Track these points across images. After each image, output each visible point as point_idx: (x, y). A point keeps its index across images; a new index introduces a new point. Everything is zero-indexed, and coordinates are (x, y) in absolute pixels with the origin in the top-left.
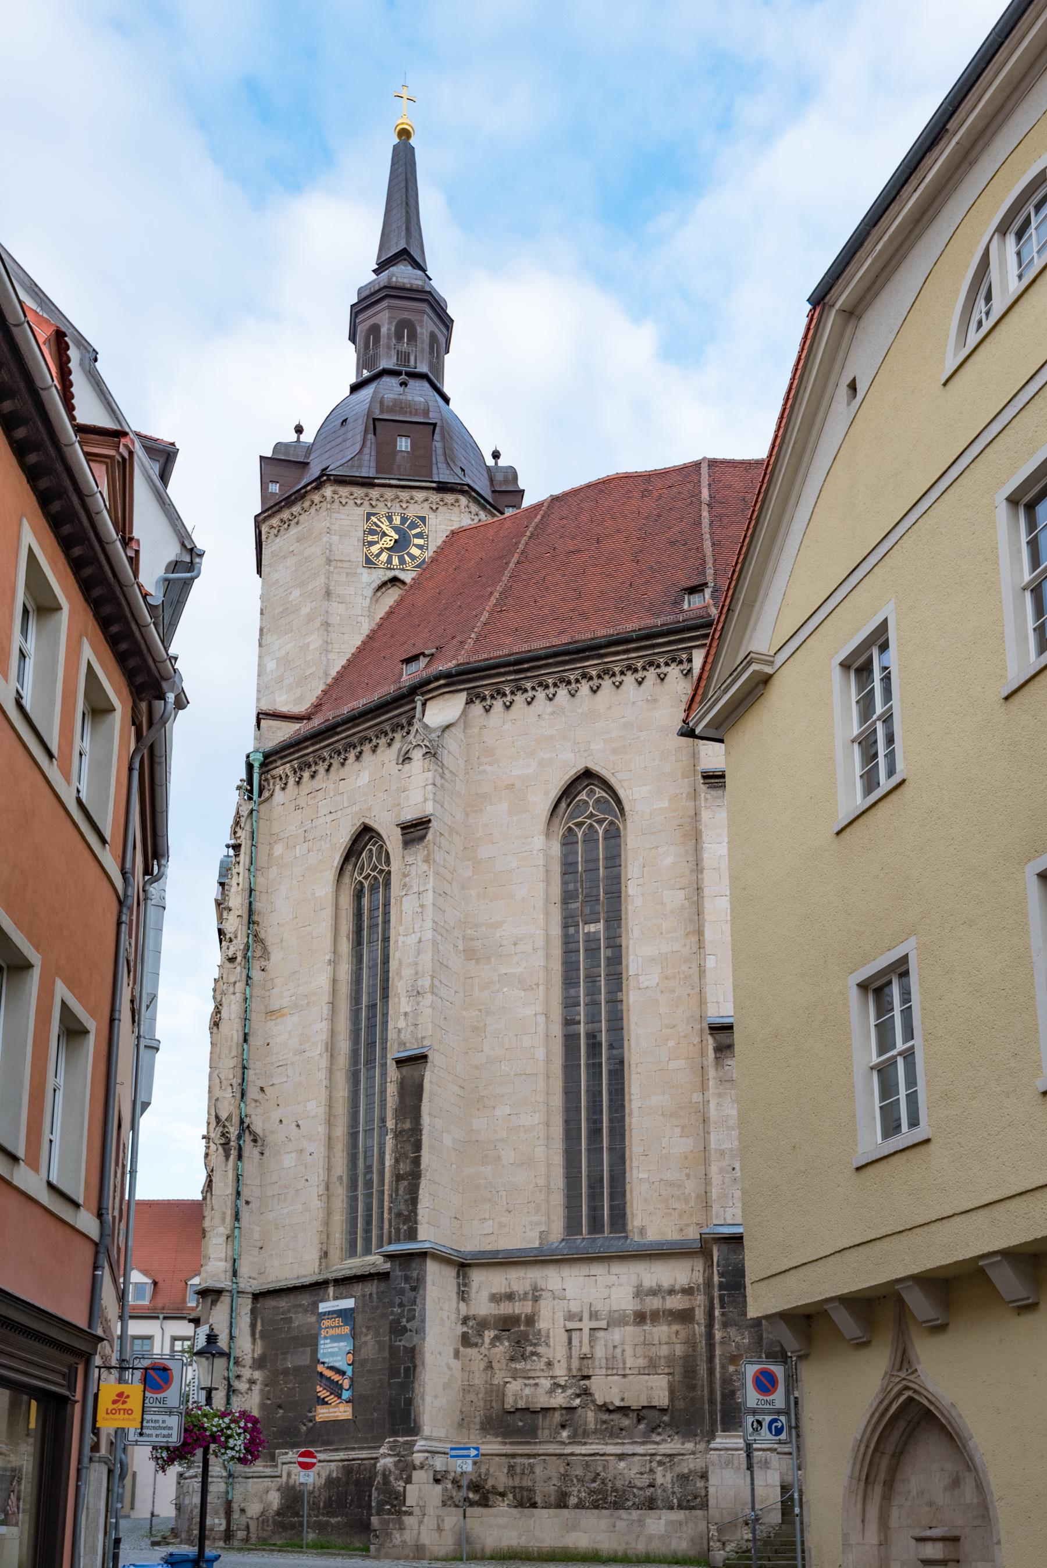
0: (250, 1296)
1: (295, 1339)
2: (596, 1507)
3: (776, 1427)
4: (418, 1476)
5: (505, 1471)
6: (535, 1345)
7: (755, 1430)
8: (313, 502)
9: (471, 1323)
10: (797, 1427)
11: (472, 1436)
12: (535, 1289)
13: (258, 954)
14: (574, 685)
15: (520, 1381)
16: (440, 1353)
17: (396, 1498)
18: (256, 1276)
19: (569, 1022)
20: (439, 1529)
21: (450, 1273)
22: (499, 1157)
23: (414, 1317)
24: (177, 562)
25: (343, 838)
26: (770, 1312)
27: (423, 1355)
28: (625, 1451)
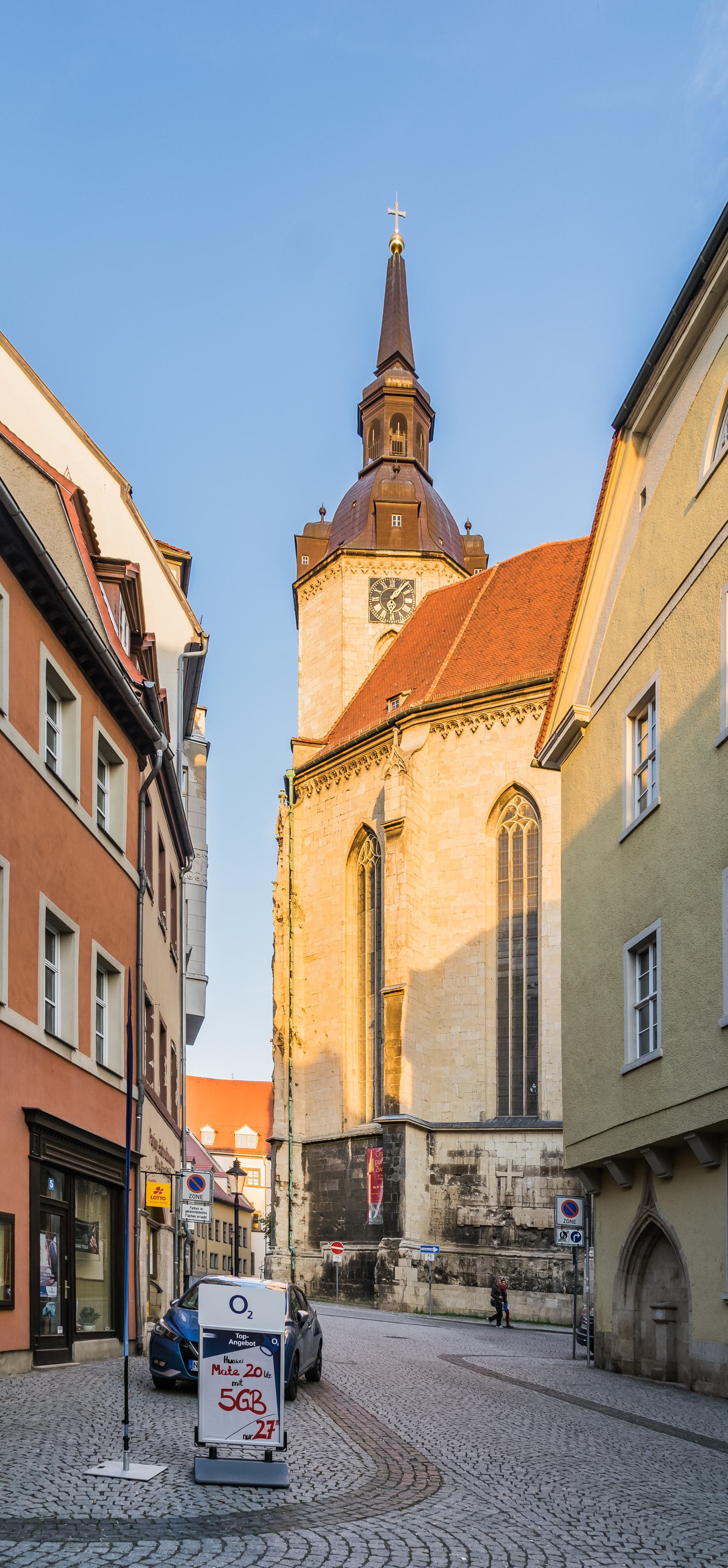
0: (301, 1145)
1: (329, 1173)
2: (515, 1289)
3: (576, 1237)
4: (401, 1261)
5: (458, 1263)
6: (477, 1185)
7: (562, 1238)
9: (436, 1169)
10: (589, 1238)
11: (437, 1240)
12: (477, 1149)
13: (297, 915)
14: (506, 718)
15: (467, 1207)
16: (415, 1187)
17: (389, 1274)
18: (304, 1132)
19: (502, 968)
20: (416, 1295)
21: (423, 1135)
22: (453, 1061)
23: (398, 1163)
24: (192, 643)
25: (349, 835)
26: (575, 1166)
27: (404, 1187)
28: (534, 1255)
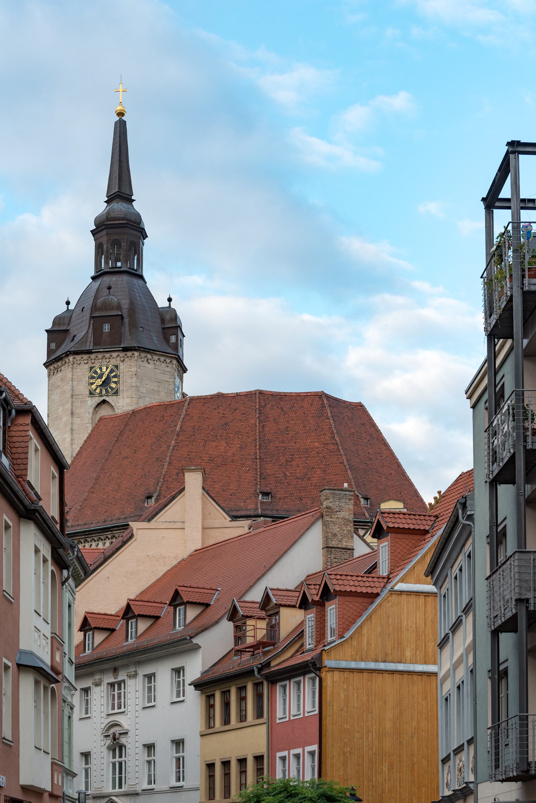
8: (66, 362)
